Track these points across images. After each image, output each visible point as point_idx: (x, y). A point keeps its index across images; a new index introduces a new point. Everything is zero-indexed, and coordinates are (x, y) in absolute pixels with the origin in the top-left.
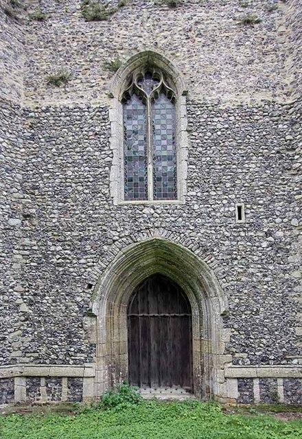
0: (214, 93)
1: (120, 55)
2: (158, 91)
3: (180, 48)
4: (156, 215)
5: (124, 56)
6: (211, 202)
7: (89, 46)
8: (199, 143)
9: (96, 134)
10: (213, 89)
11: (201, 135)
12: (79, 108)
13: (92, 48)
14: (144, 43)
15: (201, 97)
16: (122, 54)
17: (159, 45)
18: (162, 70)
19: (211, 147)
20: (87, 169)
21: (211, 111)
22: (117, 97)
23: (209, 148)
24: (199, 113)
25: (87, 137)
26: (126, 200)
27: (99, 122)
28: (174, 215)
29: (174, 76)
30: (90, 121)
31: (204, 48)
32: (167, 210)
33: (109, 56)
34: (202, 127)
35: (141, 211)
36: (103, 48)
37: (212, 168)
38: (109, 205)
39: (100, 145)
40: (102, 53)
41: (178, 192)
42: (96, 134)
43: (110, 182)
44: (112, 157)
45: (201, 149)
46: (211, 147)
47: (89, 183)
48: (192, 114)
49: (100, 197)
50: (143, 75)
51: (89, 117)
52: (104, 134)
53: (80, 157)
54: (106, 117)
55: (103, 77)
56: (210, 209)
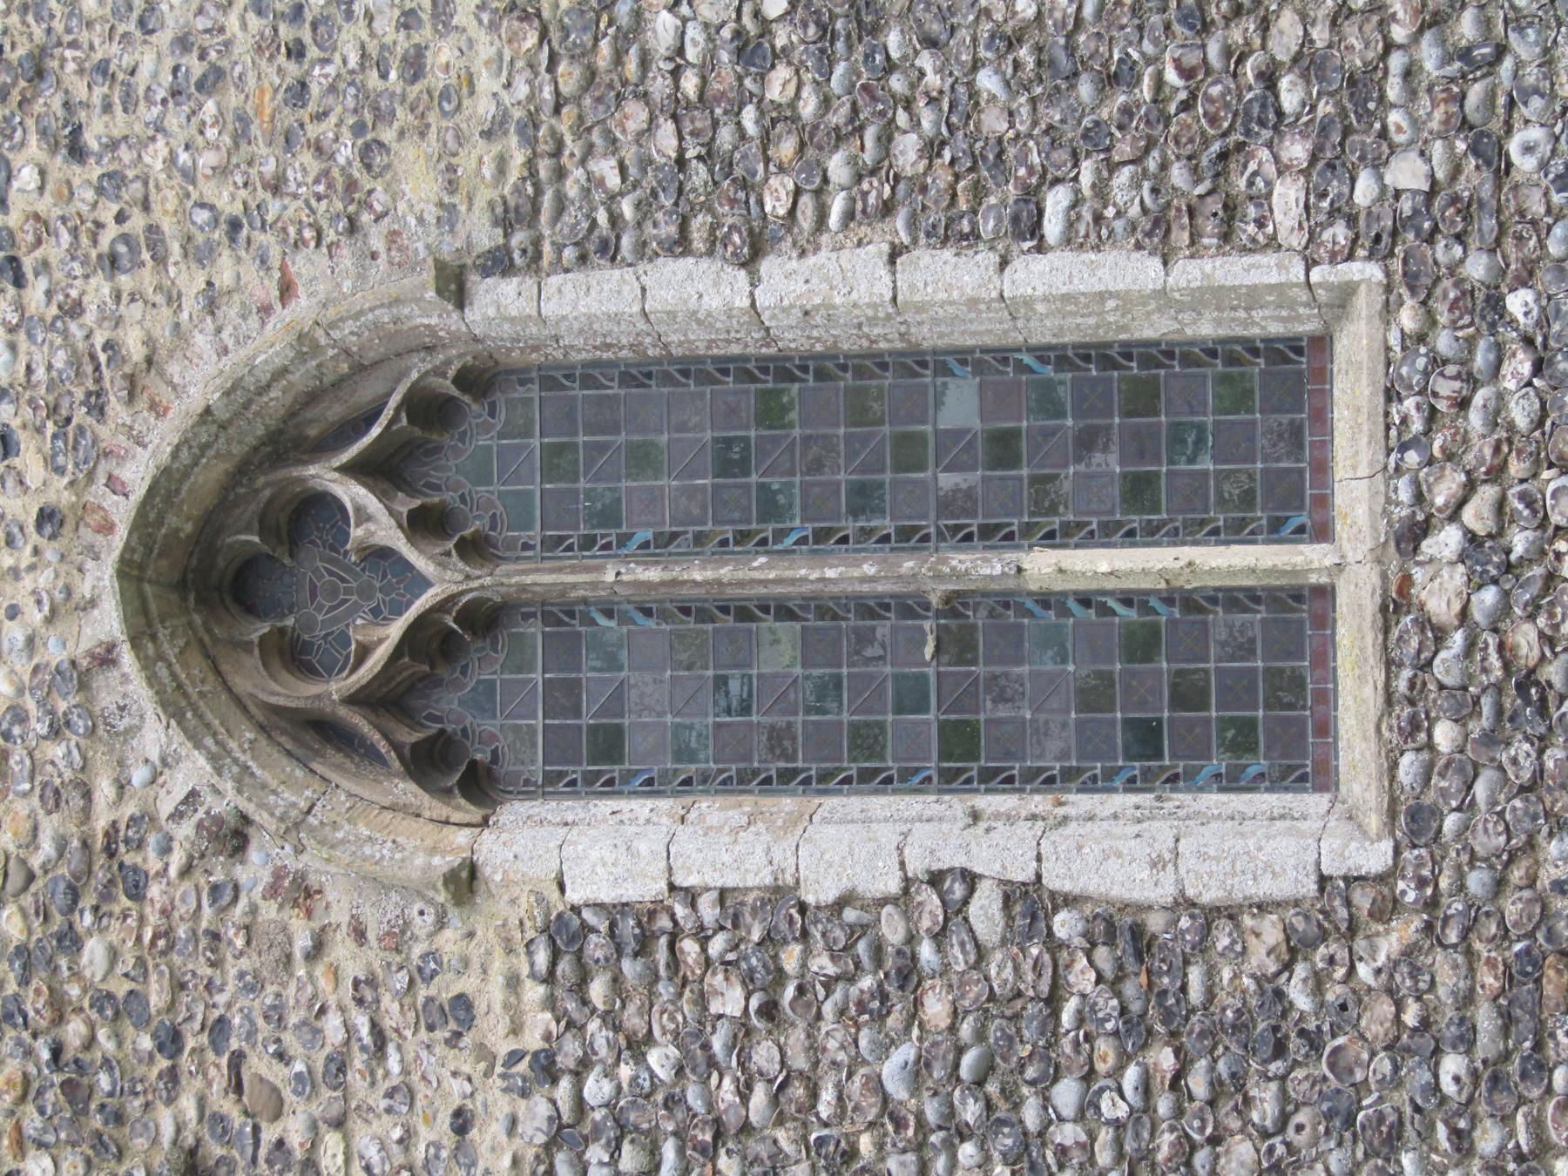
0: (443, 53)
1: (130, 809)
2: (405, 505)
3: (90, 329)
4: (1477, 514)
5: (139, 775)
6: (1358, 47)
7: (57, 1051)
8: (852, 161)
9: (770, 1011)
10: (415, 65)
11: (786, 149)
12: (550, 1147)
13: (74, 1030)
14: (36, 616)
15: (477, 159)
16: (121, 787)
17: (59, 494)
18: (243, 470)
19: (890, 67)
20: (1066, 1093)
21: (591, 74)
22: (462, 837)
23: (897, 83)
24: (606, 169)
25: (798, 1091)
26: (1321, 777)
27: (665, 990)
28: (1481, 359)
29: (301, 378)
30: (660, 1059)
31: (90, 139)
32: (1432, 415)
33: (137, 892)
34: (726, 136)
35: (1441, 636)
36: (70, 941)
37: (1071, 49)
38: (1388, 909)
39: (867, 982)
40: (114, 955)
41: (1268, 324)
42: (770, 1011)
43: (1183, 903)
44: (971, 879)
45: (907, 150)
46: (890, 67)
47: (1198, 1083)
48: (615, 220)
49: (1318, 983)
50: (265, 628)
51: (625, 1071)
52: (770, 940)
53: (967, 1151)
54: (628, 926)
55: (302, 942)
56: (1429, 55)
